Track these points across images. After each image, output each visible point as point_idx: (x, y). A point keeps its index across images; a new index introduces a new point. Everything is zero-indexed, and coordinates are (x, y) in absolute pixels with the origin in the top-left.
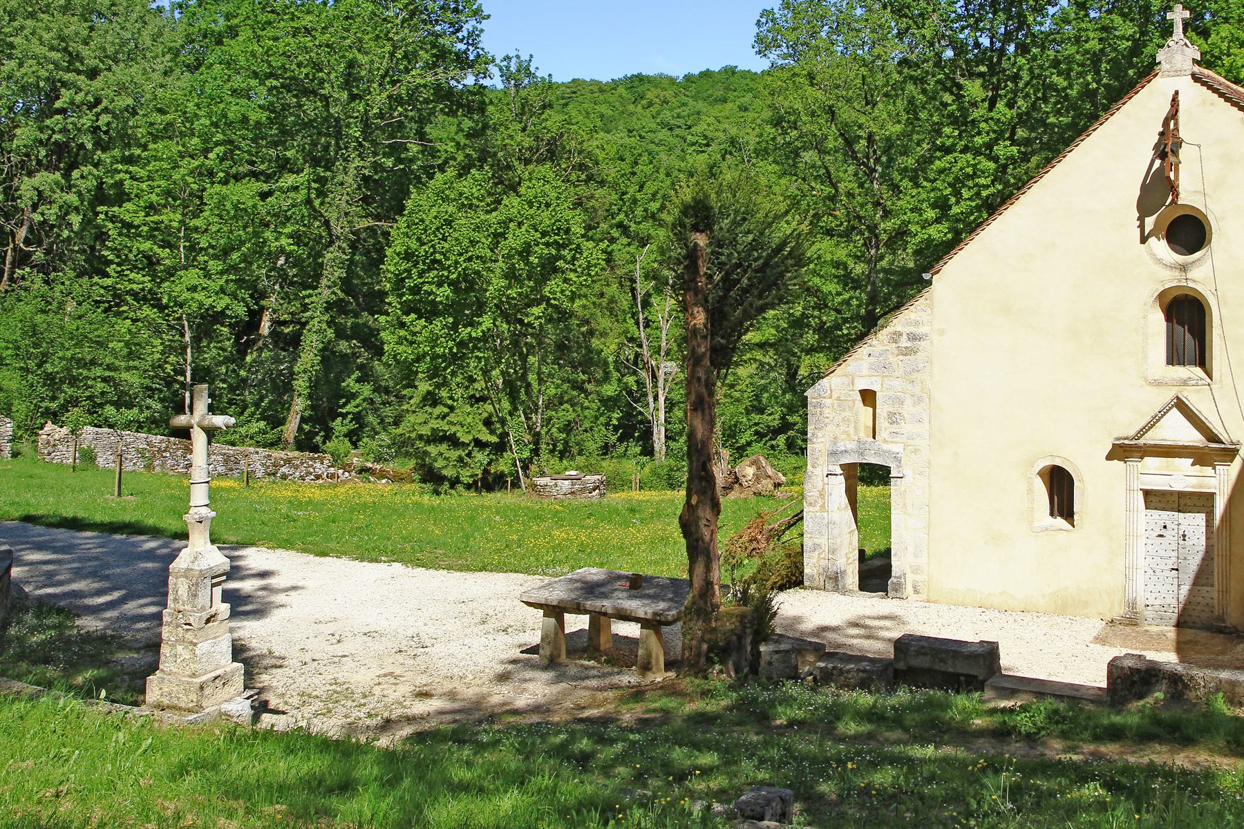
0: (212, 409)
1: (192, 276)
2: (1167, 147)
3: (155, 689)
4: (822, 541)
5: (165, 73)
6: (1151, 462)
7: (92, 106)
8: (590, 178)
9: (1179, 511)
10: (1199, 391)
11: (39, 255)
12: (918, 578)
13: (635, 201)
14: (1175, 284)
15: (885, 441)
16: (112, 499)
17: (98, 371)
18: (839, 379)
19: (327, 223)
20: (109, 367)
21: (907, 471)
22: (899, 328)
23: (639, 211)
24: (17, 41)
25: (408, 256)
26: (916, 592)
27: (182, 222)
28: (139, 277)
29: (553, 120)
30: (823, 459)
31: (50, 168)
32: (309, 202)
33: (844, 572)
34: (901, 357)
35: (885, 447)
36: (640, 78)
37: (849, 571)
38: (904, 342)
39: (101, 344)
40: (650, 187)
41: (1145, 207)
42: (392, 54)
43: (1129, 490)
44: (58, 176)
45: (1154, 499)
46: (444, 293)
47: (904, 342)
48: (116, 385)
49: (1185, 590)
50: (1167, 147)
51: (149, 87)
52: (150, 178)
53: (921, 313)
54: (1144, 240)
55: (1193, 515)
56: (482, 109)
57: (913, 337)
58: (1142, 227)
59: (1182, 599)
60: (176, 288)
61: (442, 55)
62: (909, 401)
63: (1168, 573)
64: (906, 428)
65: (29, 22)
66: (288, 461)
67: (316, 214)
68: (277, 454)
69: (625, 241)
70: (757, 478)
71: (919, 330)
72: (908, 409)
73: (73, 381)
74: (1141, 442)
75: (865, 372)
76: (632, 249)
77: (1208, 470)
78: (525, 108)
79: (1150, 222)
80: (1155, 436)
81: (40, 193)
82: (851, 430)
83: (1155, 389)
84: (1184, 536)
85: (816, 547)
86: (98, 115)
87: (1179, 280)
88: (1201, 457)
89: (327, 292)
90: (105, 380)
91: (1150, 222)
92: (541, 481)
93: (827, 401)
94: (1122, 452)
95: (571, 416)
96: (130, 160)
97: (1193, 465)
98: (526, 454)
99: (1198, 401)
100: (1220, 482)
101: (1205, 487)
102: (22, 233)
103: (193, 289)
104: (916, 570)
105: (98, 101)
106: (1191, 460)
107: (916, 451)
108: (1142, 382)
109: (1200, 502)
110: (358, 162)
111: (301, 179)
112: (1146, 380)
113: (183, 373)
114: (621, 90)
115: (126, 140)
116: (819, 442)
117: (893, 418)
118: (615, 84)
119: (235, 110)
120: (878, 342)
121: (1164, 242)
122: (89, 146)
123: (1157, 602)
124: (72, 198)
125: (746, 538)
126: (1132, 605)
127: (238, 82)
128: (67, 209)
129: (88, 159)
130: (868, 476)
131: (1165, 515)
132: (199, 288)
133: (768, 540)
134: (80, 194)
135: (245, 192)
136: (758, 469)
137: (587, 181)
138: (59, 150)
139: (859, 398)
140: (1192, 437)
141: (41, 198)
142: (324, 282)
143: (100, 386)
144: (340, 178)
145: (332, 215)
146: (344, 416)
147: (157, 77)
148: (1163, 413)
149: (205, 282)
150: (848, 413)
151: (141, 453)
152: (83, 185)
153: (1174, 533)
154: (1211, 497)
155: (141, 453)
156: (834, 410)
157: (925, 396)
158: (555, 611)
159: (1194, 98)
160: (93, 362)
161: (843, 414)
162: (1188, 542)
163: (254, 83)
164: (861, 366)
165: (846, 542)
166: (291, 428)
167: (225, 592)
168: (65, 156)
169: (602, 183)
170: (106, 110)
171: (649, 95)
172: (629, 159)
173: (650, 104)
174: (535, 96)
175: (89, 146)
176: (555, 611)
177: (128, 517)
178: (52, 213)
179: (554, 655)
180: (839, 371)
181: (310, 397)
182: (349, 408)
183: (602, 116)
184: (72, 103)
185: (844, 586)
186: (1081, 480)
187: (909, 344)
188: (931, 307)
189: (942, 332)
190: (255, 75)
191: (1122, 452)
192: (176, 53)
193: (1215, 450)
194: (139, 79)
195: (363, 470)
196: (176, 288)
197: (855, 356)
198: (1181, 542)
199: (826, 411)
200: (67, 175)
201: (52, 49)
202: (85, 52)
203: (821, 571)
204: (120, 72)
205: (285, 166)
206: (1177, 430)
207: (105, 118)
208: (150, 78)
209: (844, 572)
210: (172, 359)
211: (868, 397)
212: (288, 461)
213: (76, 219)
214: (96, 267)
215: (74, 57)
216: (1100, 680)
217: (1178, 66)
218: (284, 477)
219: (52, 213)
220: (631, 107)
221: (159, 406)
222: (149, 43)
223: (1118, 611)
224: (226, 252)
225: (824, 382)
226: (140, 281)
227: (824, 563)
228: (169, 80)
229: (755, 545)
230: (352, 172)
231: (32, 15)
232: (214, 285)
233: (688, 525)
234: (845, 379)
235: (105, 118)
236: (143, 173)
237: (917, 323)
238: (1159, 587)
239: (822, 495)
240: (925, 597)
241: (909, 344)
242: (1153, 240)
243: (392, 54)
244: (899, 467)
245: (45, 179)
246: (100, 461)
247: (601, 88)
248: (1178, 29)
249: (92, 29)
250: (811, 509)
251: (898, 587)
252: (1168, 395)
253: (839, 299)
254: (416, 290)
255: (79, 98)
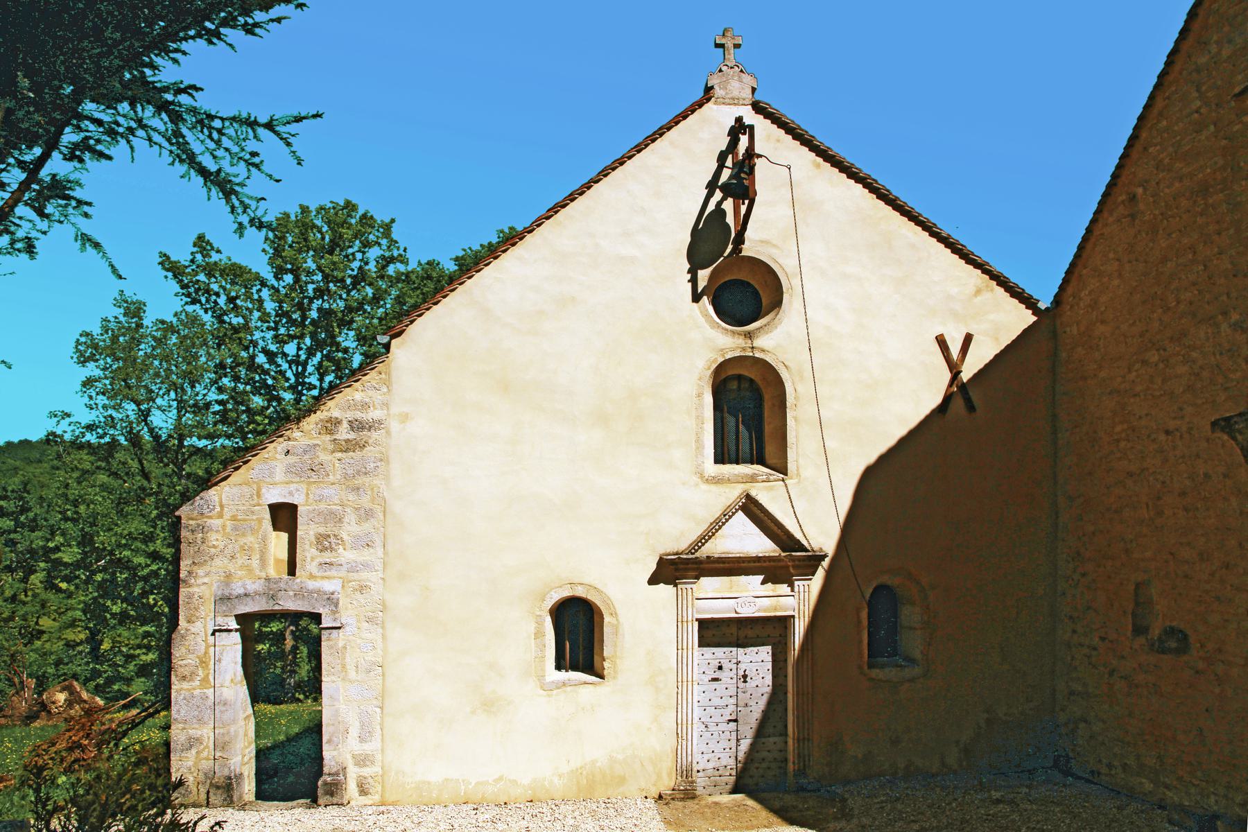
2: (737, 178)
4: (206, 733)
6: (709, 585)
9: (738, 646)
10: (771, 488)
12: (366, 771)
14: (737, 354)
15: (312, 577)
18: (235, 490)
21: (347, 615)
22: (336, 413)
26: (363, 792)
30: (207, 609)
33: (239, 777)
34: (339, 455)
35: (311, 585)
37: (246, 774)
38: (344, 433)
41: (697, 257)
43: (680, 621)
45: (715, 632)
47: (344, 433)
49: (745, 745)
53: (370, 393)
55: (755, 649)
58: (694, 281)
59: (741, 756)
62: (350, 517)
63: (723, 727)
64: (346, 555)
70: (69, 703)
71: (374, 414)
72: (350, 528)
74: (705, 551)
75: (279, 475)
77: (784, 589)
79: (704, 275)
80: (721, 546)
82: (255, 563)
83: (713, 487)
84: (745, 676)
85: (192, 743)
87: (744, 349)
88: (772, 571)
91: (704, 275)
93: (215, 523)
94: (672, 570)
97: (763, 583)
99: (771, 497)
100: (797, 601)
101: (782, 609)
104: (362, 761)
106: (761, 577)
107: (362, 589)
108: (696, 479)
109: (767, 631)
112: (702, 476)
116: (201, 586)
117: (324, 543)
120: (305, 434)
123: (711, 765)
125: (62, 745)
126: (686, 773)
131: (720, 651)
133: (99, 746)
136: (71, 694)
139: (268, 516)
140: (759, 544)
148: (726, 516)
150: (250, 539)
153: (733, 674)
154: (784, 622)
156: (225, 535)
157: (378, 509)
161: (242, 541)
162: (751, 684)
164: (271, 474)
165: (241, 733)
180: (236, 477)
185: (241, 797)
186: (614, 614)
187: (352, 436)
188: (388, 383)
189: (405, 418)
191: (672, 570)
193: (788, 560)
197: (264, 454)
198: (741, 685)
199: (213, 538)
203: (201, 777)
206: (745, 539)
209: (239, 777)
211: (284, 516)
217: (735, 93)
223: (667, 782)
225: (213, 494)
227: (206, 765)
229: (77, 754)
234: (245, 489)
237: (365, 406)
238: (712, 746)
239: (203, 663)
240: (377, 798)
241: (352, 436)
244: (334, 612)
250: (185, 685)
251: (334, 789)
252: (733, 494)
253: (146, 571)
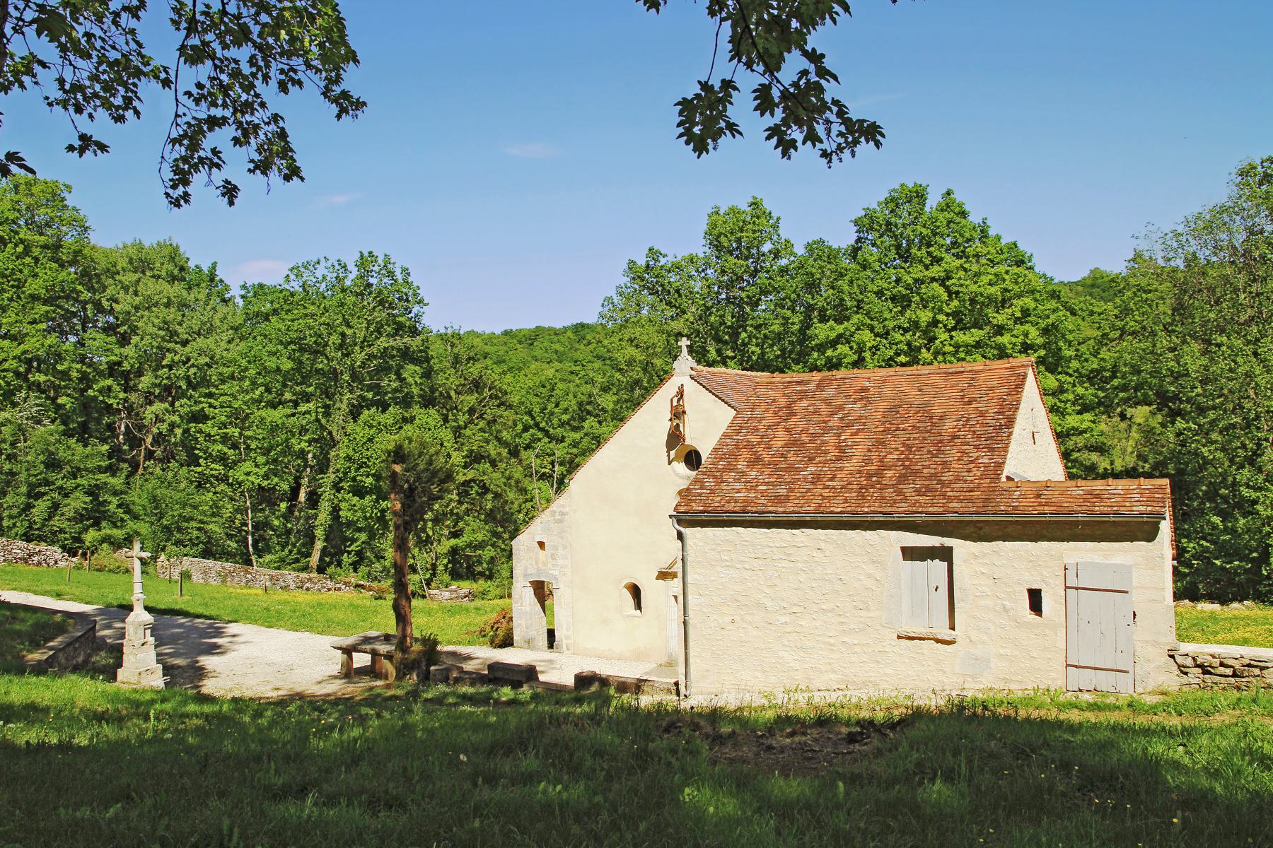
0: (142, 549)
1: (248, 466)
3: (121, 673)
5: (229, 342)
7: (184, 363)
8: (502, 404)
11: (158, 453)
13: (552, 414)
16: (177, 597)
17: (194, 524)
19: (330, 433)
20: (201, 522)
21: (561, 586)
23: (555, 421)
24: (140, 324)
25: (349, 458)
27: (241, 434)
28: (217, 467)
29: (475, 370)
31: (162, 400)
32: (318, 420)
36: (582, 326)
39: (195, 507)
40: (564, 405)
42: (367, 328)
44: (167, 405)
46: (369, 481)
47: (558, 517)
48: (206, 532)
50: (678, 414)
51: (218, 351)
52: (222, 407)
54: (670, 463)
56: (428, 360)
57: (562, 514)
60: (238, 474)
61: (399, 328)
65: (147, 313)
66: (310, 580)
67: (323, 428)
68: (304, 575)
69: (546, 440)
72: (561, 552)
73: (179, 529)
76: (551, 446)
78: (456, 361)
79: (672, 453)
81: (157, 417)
86: (188, 369)
89: (333, 476)
90: (199, 529)
92: (433, 592)
95: (493, 554)
96: (210, 395)
98: (428, 576)
102: (149, 440)
103: (248, 474)
104: (567, 638)
105: (188, 359)
110: (348, 396)
111: (311, 406)
113: (246, 525)
114: (569, 334)
115: (205, 382)
118: (565, 330)
119: (271, 363)
121: (683, 465)
122: (184, 387)
124: (176, 418)
127: (271, 347)
128: (172, 426)
129: (184, 395)
130: (541, 591)
132: (250, 473)
134: (180, 416)
135: (277, 415)
137: (498, 406)
138: (167, 389)
141: (158, 419)
142: (331, 470)
143: (195, 533)
144: (338, 405)
145: (334, 429)
146: (349, 553)
147: (223, 344)
149: (255, 470)
151: (219, 574)
152: (182, 410)
155: (219, 574)
158: (348, 651)
159: (691, 388)
160: (192, 519)
163: (280, 347)
166: (314, 560)
167: (386, 678)
168: (169, 392)
169: (510, 406)
170: (193, 366)
171: (588, 337)
172: (548, 386)
173: (589, 343)
174: (464, 350)
175: (184, 387)
176: (348, 651)
177: (177, 607)
178: (164, 427)
179: (349, 673)
181: (326, 540)
182: (353, 548)
183: (556, 351)
184: (173, 360)
190: (281, 343)
192: (236, 329)
194: (212, 346)
195: (358, 586)
196: (238, 474)
200: (172, 404)
201: (160, 329)
202: (180, 330)
204: (201, 342)
205: (307, 398)
207: (192, 370)
208: (217, 344)
210: (239, 516)
211: (541, 545)
212: (310, 580)
213: (178, 432)
214: (194, 461)
215: (173, 334)
216: (570, 681)
218: (308, 589)
219: (164, 427)
220: (577, 346)
221: (235, 545)
222: (218, 323)
223: (664, 660)
224: (269, 451)
226: (218, 468)
228: (231, 346)
230: (345, 402)
231: (148, 308)
232: (262, 471)
233: (396, 607)
235: (192, 370)
236: (216, 403)
242: (674, 463)
243: (367, 328)
245: (159, 407)
246: (194, 578)
247: (556, 333)
248: (685, 350)
249: (183, 316)
254: (354, 479)
255: (177, 358)
